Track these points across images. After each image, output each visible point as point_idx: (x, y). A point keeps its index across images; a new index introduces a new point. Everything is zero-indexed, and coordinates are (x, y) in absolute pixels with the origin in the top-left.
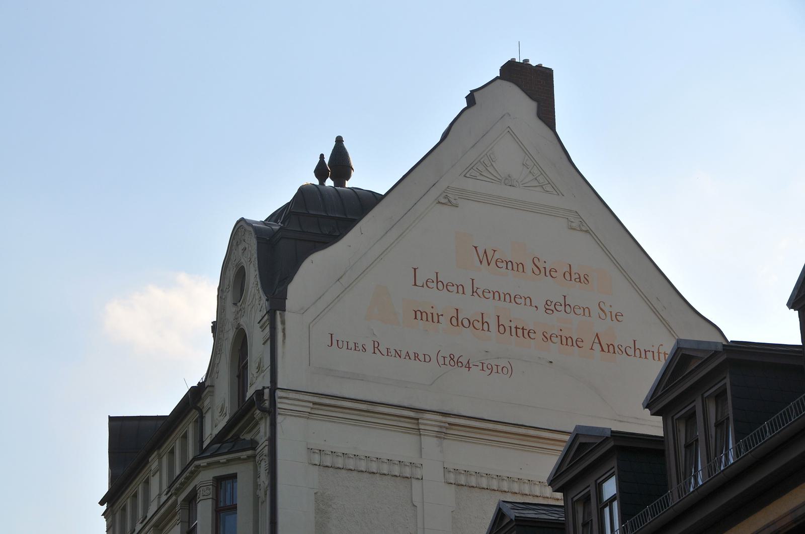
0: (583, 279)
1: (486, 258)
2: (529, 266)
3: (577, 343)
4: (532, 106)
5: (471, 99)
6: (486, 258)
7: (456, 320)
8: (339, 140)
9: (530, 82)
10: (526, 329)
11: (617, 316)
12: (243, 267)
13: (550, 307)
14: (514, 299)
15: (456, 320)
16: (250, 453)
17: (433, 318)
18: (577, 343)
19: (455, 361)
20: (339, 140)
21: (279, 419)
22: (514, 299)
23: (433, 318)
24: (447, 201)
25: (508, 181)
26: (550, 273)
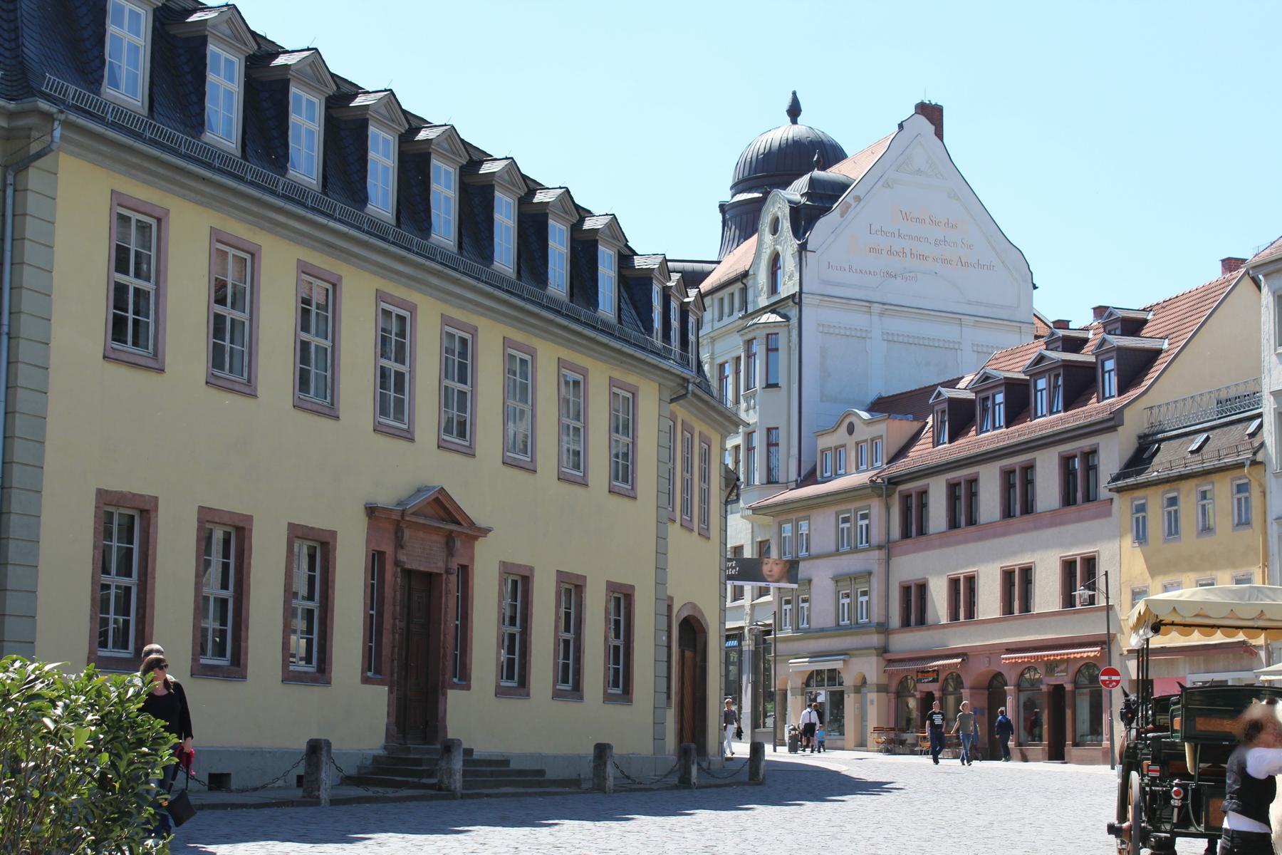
0: (954, 227)
1: (906, 217)
2: (928, 221)
3: (949, 262)
4: (933, 128)
5: (901, 126)
6: (906, 217)
7: (890, 252)
8: (794, 93)
9: (932, 113)
10: (1148, 640)
11: (970, 247)
12: (778, 218)
13: (937, 243)
14: (919, 239)
15: (890, 252)
16: (1157, 642)
17: (880, 251)
18: (949, 262)
19: (889, 274)
20: (794, 93)
21: (804, 308)
22: (919, 239)
23: (880, 251)
24: (888, 185)
25: (919, 172)
26: (938, 224)
